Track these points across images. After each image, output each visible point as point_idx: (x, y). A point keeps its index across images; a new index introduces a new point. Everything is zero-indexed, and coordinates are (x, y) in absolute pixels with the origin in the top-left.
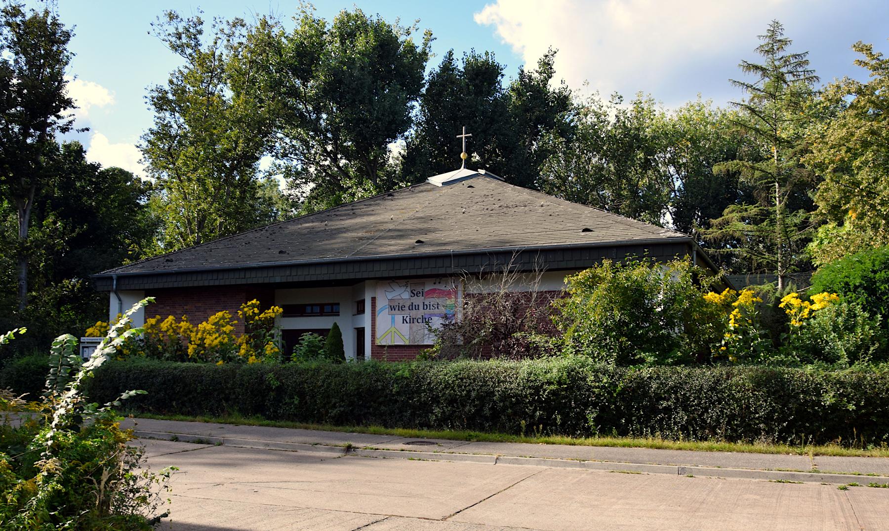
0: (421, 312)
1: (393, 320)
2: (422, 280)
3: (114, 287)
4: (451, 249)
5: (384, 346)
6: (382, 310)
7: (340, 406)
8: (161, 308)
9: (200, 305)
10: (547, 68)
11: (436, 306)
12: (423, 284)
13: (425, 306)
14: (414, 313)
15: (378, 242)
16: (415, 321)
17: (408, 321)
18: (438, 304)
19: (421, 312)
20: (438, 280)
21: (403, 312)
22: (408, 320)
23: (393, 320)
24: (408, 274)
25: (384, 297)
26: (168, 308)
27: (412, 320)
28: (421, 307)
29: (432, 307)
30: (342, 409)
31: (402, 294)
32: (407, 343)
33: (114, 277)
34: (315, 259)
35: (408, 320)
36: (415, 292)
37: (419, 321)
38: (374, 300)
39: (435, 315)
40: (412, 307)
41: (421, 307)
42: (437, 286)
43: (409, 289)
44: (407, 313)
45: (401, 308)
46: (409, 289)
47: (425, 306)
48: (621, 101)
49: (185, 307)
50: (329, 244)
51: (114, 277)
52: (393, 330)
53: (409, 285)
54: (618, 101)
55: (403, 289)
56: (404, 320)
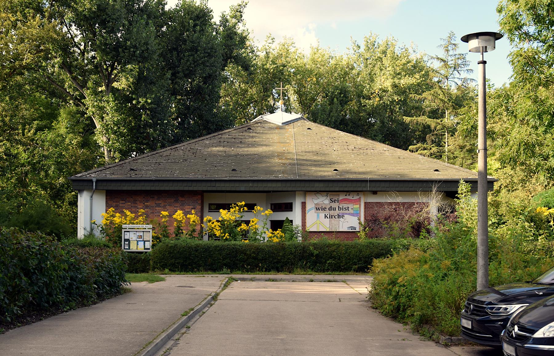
0: (337, 212)
1: (318, 216)
2: (338, 193)
3: (94, 187)
4: (368, 177)
5: (333, 232)
6: (310, 210)
7: (359, 264)
8: (122, 203)
9: (160, 202)
10: (238, 14)
11: (347, 209)
12: (339, 195)
13: (340, 209)
14: (332, 212)
15: (303, 167)
16: (333, 217)
17: (329, 217)
18: (348, 208)
19: (337, 212)
20: (348, 194)
21: (325, 212)
22: (328, 216)
23: (318, 216)
24: (338, 190)
25: (311, 202)
26: (130, 204)
27: (331, 217)
28: (337, 209)
29: (344, 209)
30: (360, 265)
31: (324, 201)
32: (328, 230)
33: (94, 180)
34: (272, 178)
35: (328, 216)
36: (333, 200)
37: (336, 217)
38: (304, 205)
39: (346, 214)
40: (331, 209)
41: (337, 209)
42: (348, 197)
43: (329, 198)
44: (327, 212)
45: (324, 209)
46: (329, 198)
47: (340, 209)
48: (273, 42)
49: (146, 204)
50: (320, 171)
51: (94, 180)
52: (318, 222)
53: (329, 196)
54: (271, 41)
55: (325, 198)
56: (326, 216)
